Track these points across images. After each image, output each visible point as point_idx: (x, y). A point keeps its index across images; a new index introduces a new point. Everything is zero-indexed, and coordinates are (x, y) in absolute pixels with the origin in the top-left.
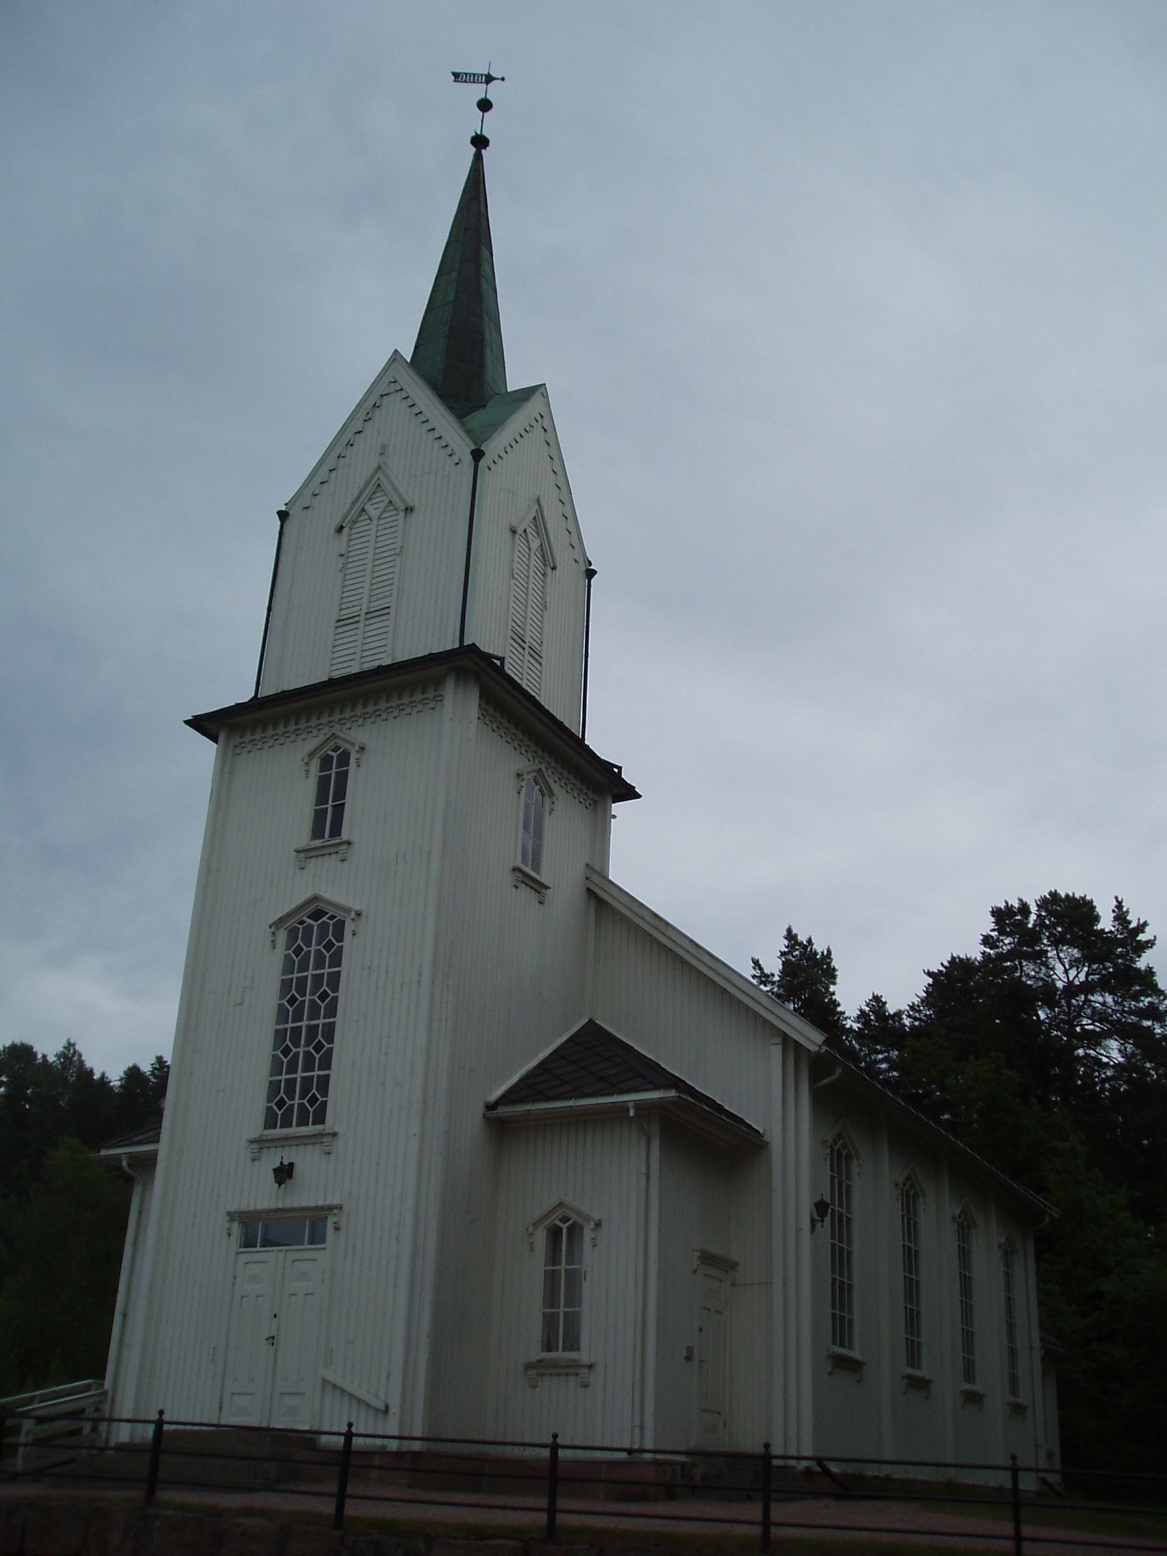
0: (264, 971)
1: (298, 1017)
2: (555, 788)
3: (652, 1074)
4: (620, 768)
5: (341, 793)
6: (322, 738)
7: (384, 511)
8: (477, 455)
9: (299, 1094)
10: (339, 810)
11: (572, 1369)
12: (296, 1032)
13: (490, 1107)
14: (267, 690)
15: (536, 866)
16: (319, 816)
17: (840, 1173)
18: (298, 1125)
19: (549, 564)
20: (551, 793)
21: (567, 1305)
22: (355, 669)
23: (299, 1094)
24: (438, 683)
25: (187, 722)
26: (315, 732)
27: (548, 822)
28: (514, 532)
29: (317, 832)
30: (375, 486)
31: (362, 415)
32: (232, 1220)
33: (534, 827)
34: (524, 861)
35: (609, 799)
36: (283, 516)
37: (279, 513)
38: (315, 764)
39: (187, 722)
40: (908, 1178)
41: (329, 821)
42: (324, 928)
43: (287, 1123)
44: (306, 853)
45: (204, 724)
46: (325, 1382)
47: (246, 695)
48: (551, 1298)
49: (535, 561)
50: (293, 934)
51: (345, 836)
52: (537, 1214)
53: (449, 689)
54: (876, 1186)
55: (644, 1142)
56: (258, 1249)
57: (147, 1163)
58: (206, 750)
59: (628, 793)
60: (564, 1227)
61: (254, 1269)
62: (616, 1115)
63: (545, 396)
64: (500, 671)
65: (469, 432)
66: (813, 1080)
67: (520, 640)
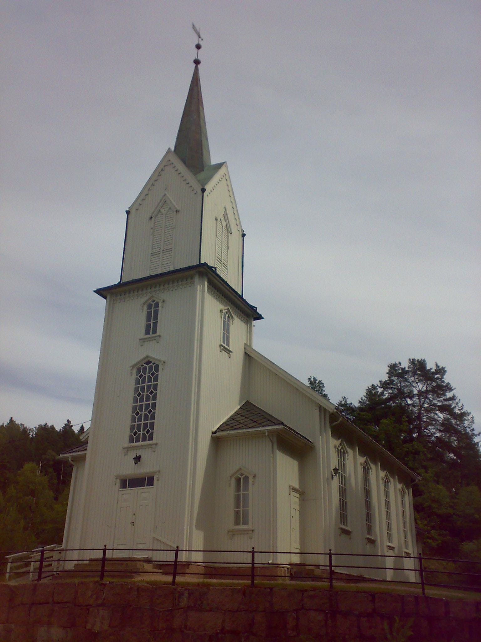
0: (128, 384)
1: (142, 400)
3: (271, 420)
4: (256, 308)
5: (156, 317)
6: (148, 297)
8: (203, 190)
10: (155, 324)
11: (245, 532)
12: (141, 406)
13: (214, 433)
14: (125, 280)
15: (228, 345)
16: (148, 327)
17: (341, 458)
18: (142, 441)
20: (232, 318)
23: (143, 429)
24: (192, 277)
25: (94, 291)
26: (145, 295)
27: (231, 327)
28: (216, 219)
29: (147, 332)
30: (164, 202)
32: (116, 478)
34: (224, 342)
35: (253, 319)
36: (128, 213)
38: (146, 307)
39: (94, 291)
40: (365, 462)
41: (151, 328)
42: (151, 368)
43: (138, 441)
44: (143, 340)
45: (101, 292)
46: (154, 538)
47: (117, 281)
48: (237, 505)
49: (224, 231)
50: (139, 370)
51: (158, 334)
53: (196, 279)
54: (354, 461)
55: (271, 444)
56: (127, 489)
57: (83, 458)
58: (102, 302)
59: (259, 317)
60: (242, 477)
62: (262, 434)
63: (227, 167)
64: (215, 272)
65: (199, 181)
66: (331, 422)
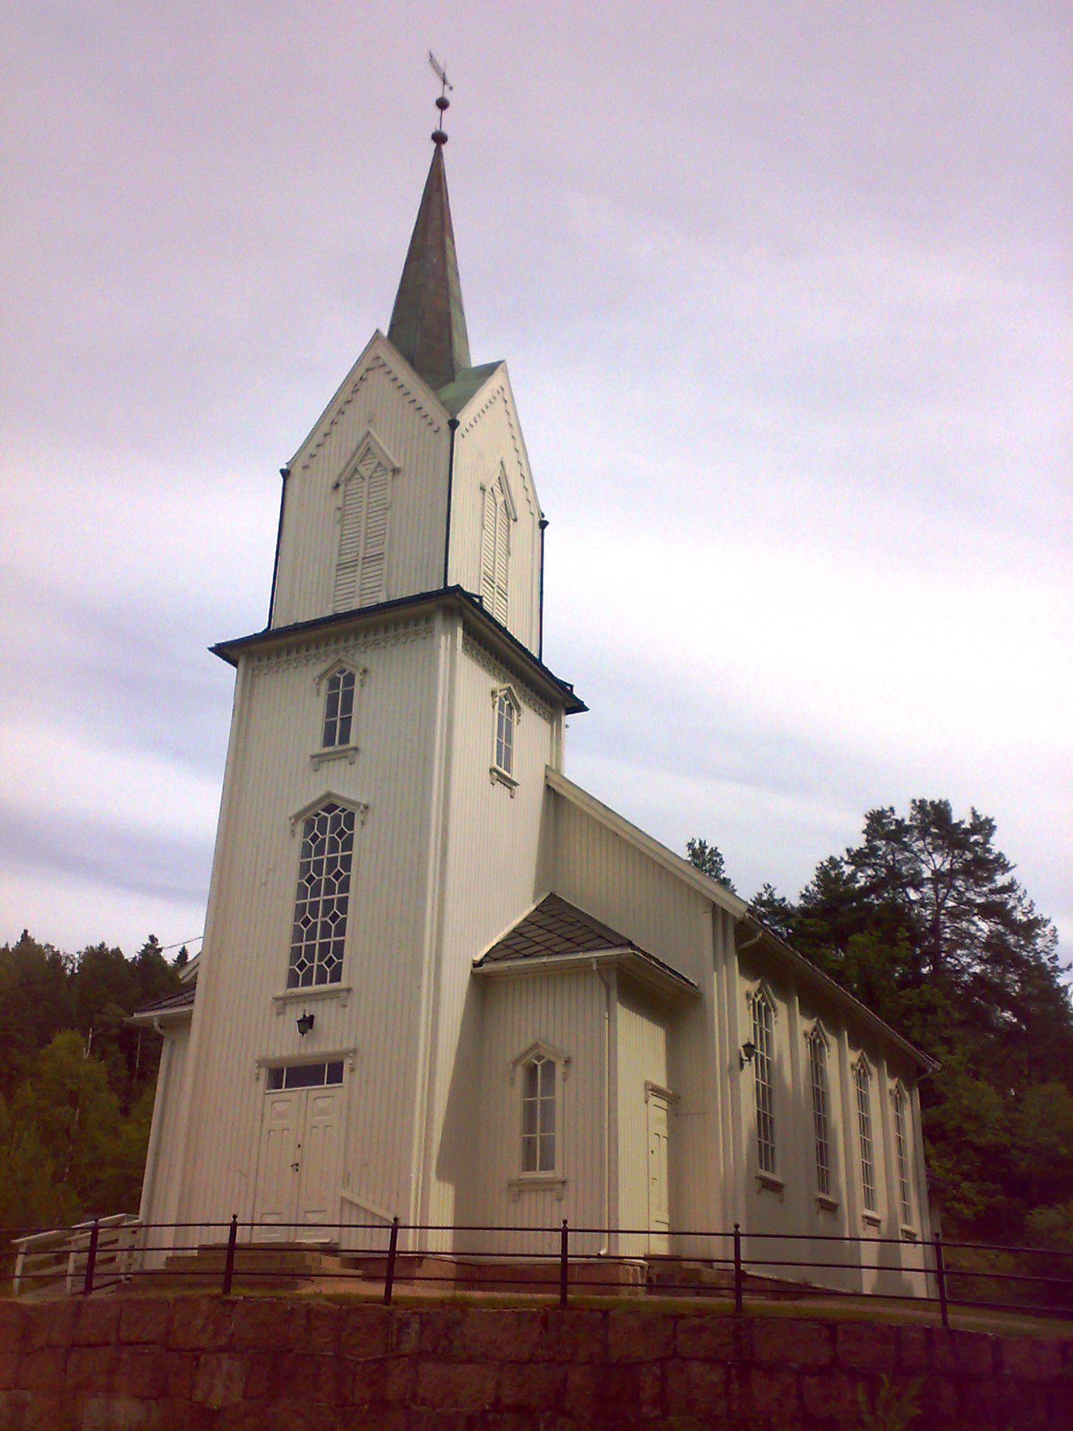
0: (285, 857)
1: (316, 893)
2: (522, 705)
4: (572, 687)
5: (348, 707)
7: (375, 471)
8: (454, 424)
9: (318, 956)
10: (347, 722)
12: (315, 905)
13: (476, 965)
14: (279, 623)
15: (508, 769)
17: (761, 1021)
18: (318, 983)
19: (510, 515)
20: (518, 708)
21: (543, 1131)
22: (355, 605)
23: (318, 956)
24: (428, 618)
25: (211, 649)
27: (516, 730)
28: (483, 489)
29: (328, 740)
30: (366, 450)
31: (350, 387)
32: (259, 1067)
33: (505, 733)
34: (499, 763)
36: (285, 474)
37: (282, 472)
38: (325, 685)
39: (211, 649)
41: (337, 731)
42: (336, 820)
43: (307, 982)
45: (224, 651)
46: (343, 1199)
47: (261, 626)
48: (530, 1125)
49: (501, 516)
50: (309, 825)
51: (352, 744)
52: (517, 1053)
53: (438, 623)
55: (604, 991)
58: (227, 674)
59: (579, 707)
60: (539, 1064)
61: (279, 1107)
63: (506, 371)
64: (479, 607)
65: (444, 404)
66: (738, 942)
67: (490, 580)
